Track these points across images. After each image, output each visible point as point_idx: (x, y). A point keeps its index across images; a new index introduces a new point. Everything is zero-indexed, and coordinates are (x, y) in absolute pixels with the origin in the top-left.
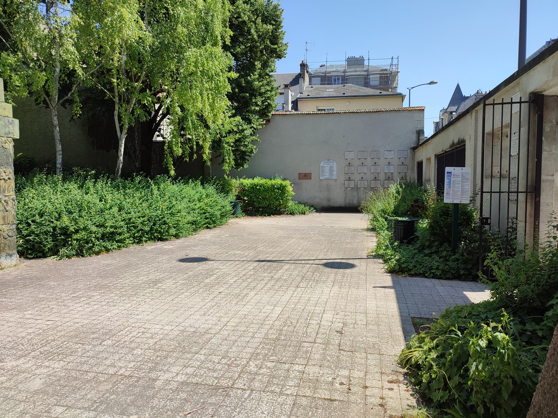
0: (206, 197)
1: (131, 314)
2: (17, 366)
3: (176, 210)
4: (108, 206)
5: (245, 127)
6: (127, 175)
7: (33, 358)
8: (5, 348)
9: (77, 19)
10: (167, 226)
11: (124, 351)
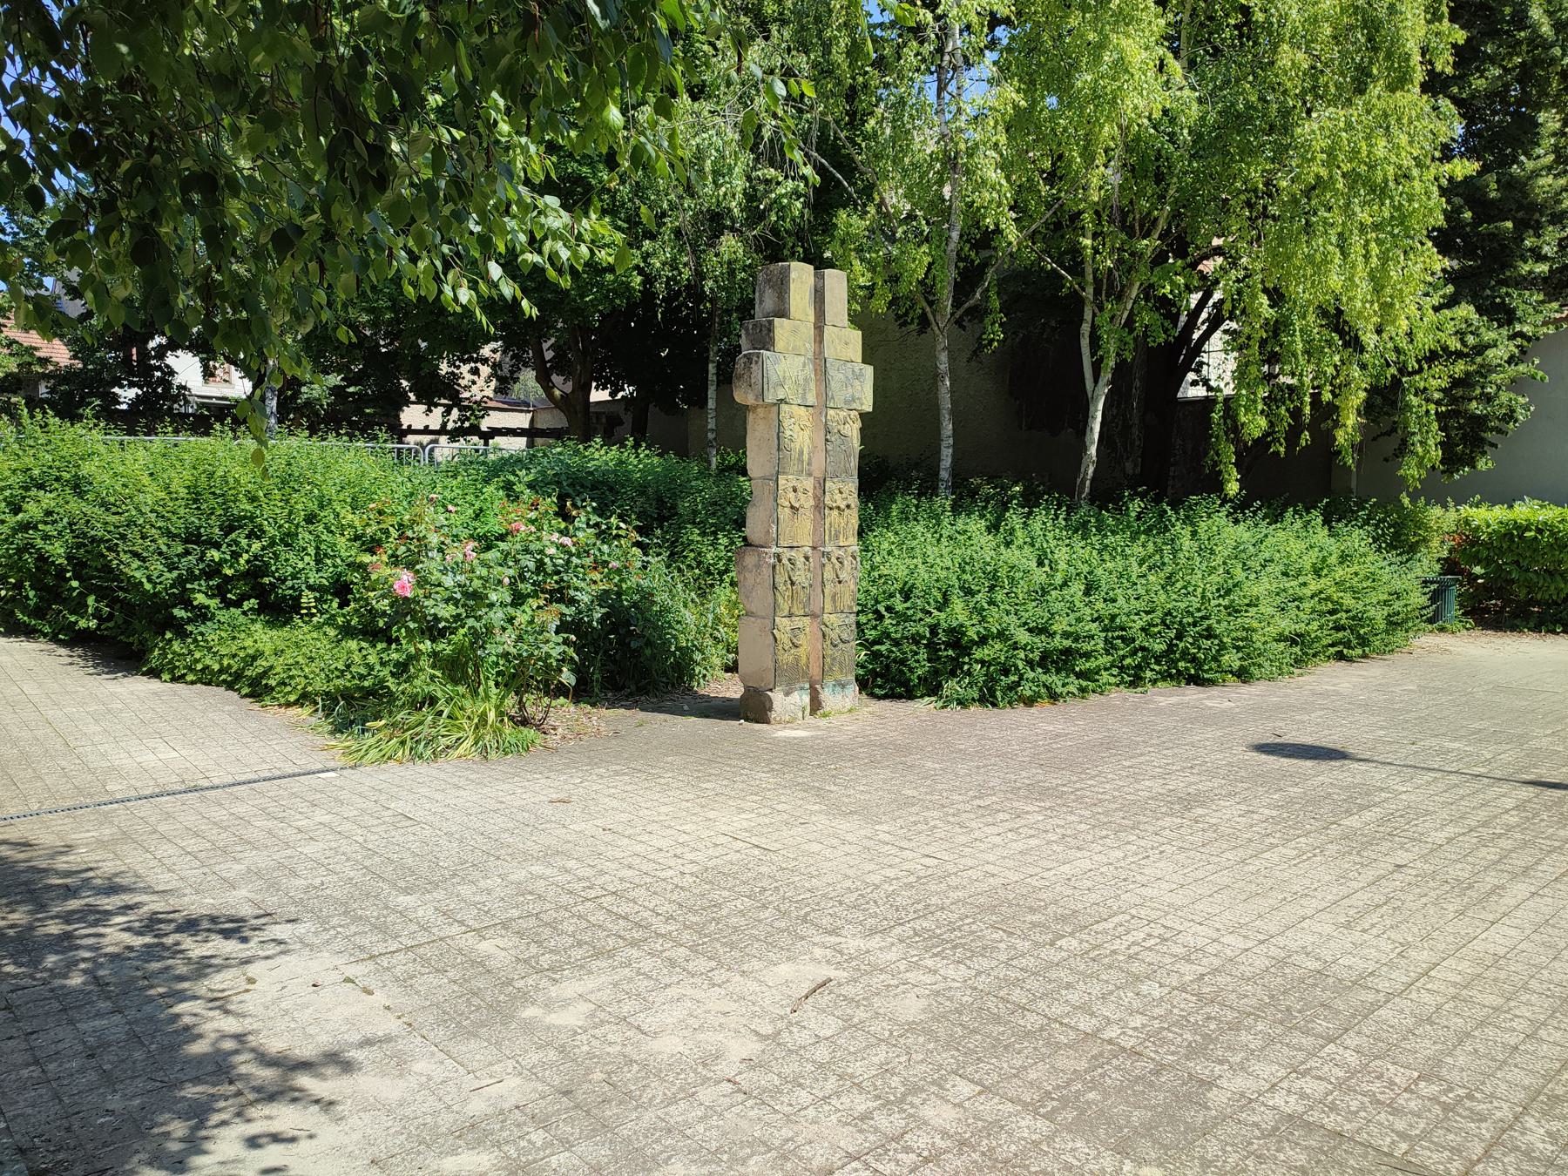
0: (1340, 563)
1: (1125, 880)
2: (868, 951)
3: (1244, 597)
4: (1058, 579)
5: (1489, 336)
6: (1106, 495)
7: (901, 941)
8: (841, 903)
9: (1011, 94)
10: (1216, 642)
11: (1113, 976)
